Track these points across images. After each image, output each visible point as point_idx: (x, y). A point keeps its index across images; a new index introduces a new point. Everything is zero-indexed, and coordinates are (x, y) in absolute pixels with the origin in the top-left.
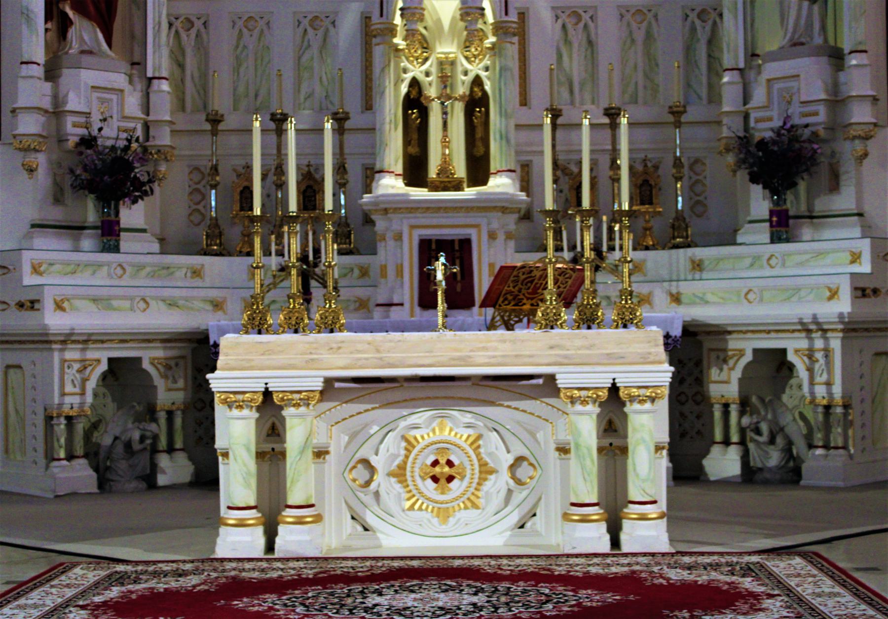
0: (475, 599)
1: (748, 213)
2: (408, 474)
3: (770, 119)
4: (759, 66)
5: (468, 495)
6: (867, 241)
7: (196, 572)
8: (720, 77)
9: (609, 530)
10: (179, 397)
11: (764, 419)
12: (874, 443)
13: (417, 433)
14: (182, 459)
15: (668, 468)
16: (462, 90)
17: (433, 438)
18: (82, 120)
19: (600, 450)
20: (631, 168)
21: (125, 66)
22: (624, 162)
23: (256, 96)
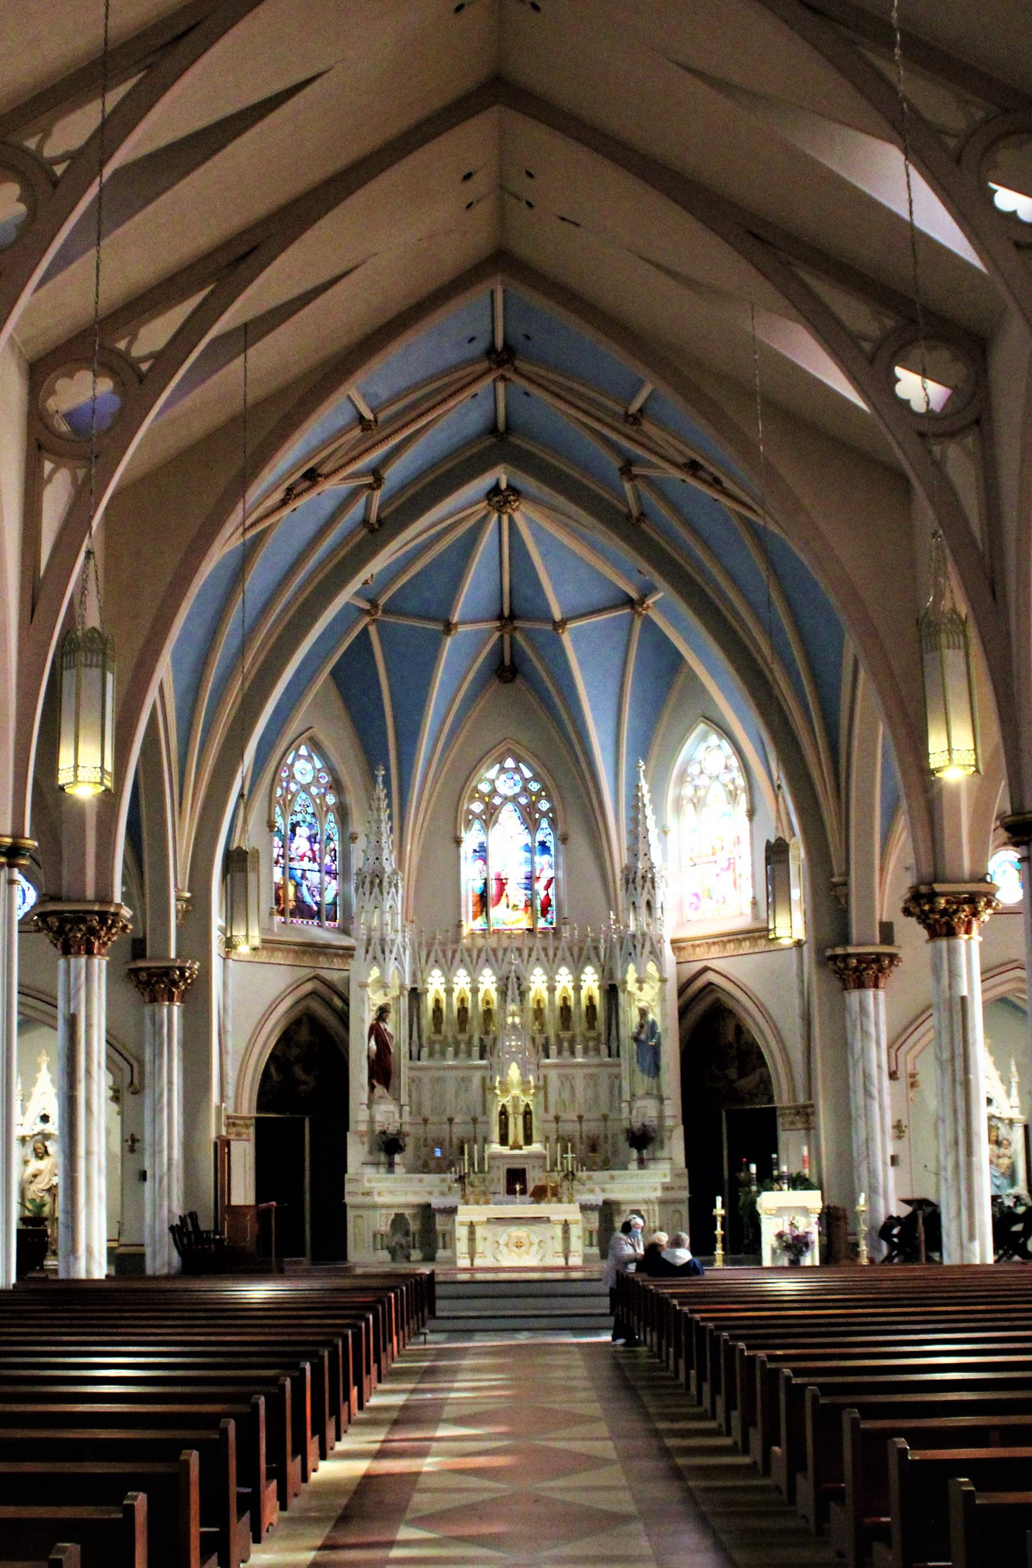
16: (522, 1109)
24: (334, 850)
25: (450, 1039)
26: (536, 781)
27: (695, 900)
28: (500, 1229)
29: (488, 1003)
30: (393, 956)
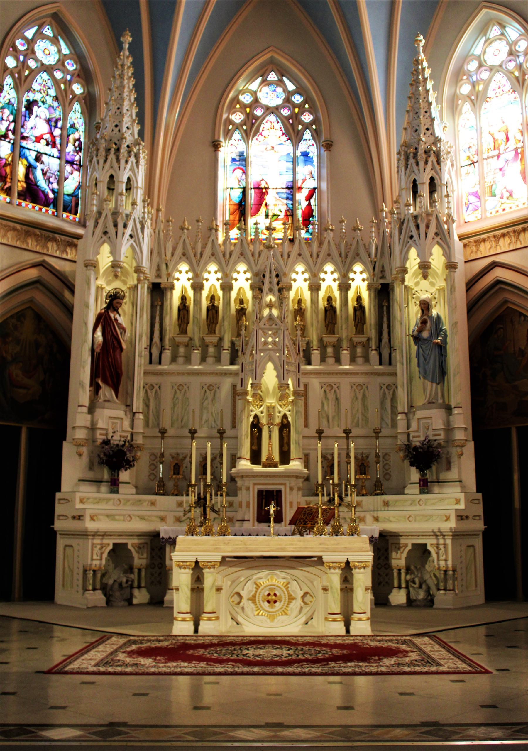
0: (288, 652)
1: (410, 480)
2: (257, 599)
3: (419, 436)
4: (414, 412)
5: (283, 609)
6: (463, 494)
7: (165, 640)
8: (397, 417)
9: (345, 625)
10: (144, 562)
11: (417, 576)
12: (467, 588)
13: (261, 581)
14: (144, 591)
15: (371, 600)
16: (278, 421)
17: (268, 583)
18: (104, 432)
19: (342, 590)
20: (356, 457)
21: (123, 407)
22: (352, 455)
23: (182, 421)
24: (79, 140)
25: (197, 342)
26: (299, 93)
27: (473, 199)
28: (243, 574)
29: (242, 302)
30: (128, 232)
